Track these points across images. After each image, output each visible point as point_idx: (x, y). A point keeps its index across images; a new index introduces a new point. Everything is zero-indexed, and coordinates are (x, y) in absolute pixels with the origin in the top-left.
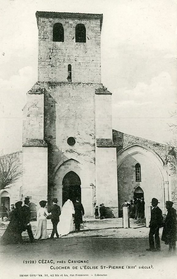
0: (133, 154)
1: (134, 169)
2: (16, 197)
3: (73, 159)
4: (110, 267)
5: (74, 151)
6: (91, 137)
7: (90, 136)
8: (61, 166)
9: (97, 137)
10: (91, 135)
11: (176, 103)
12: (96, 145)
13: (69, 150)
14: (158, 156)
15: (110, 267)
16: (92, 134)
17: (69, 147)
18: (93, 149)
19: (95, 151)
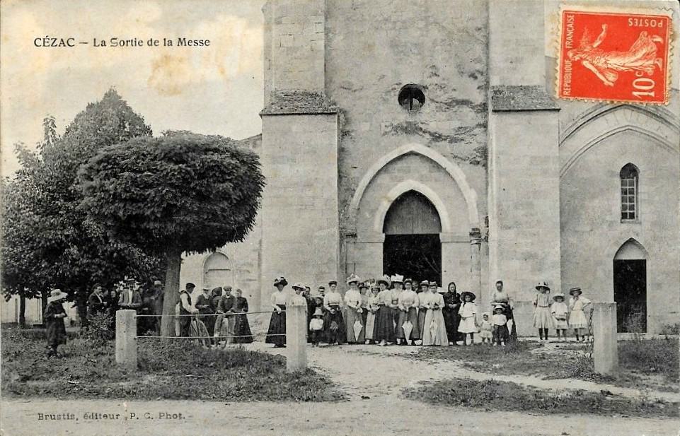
0: (589, 147)
1: (618, 181)
2: (248, 271)
3: (417, 154)
4: (133, 415)
5: (421, 129)
6: (476, 84)
7: (472, 79)
8: (379, 172)
9: (495, 82)
10: (476, 78)
11: (676, 211)
12: (490, 108)
13: (405, 125)
14: (589, 111)
15: (133, 415)
16: (477, 74)
17: (402, 116)
18: (482, 122)
19: (485, 126)
